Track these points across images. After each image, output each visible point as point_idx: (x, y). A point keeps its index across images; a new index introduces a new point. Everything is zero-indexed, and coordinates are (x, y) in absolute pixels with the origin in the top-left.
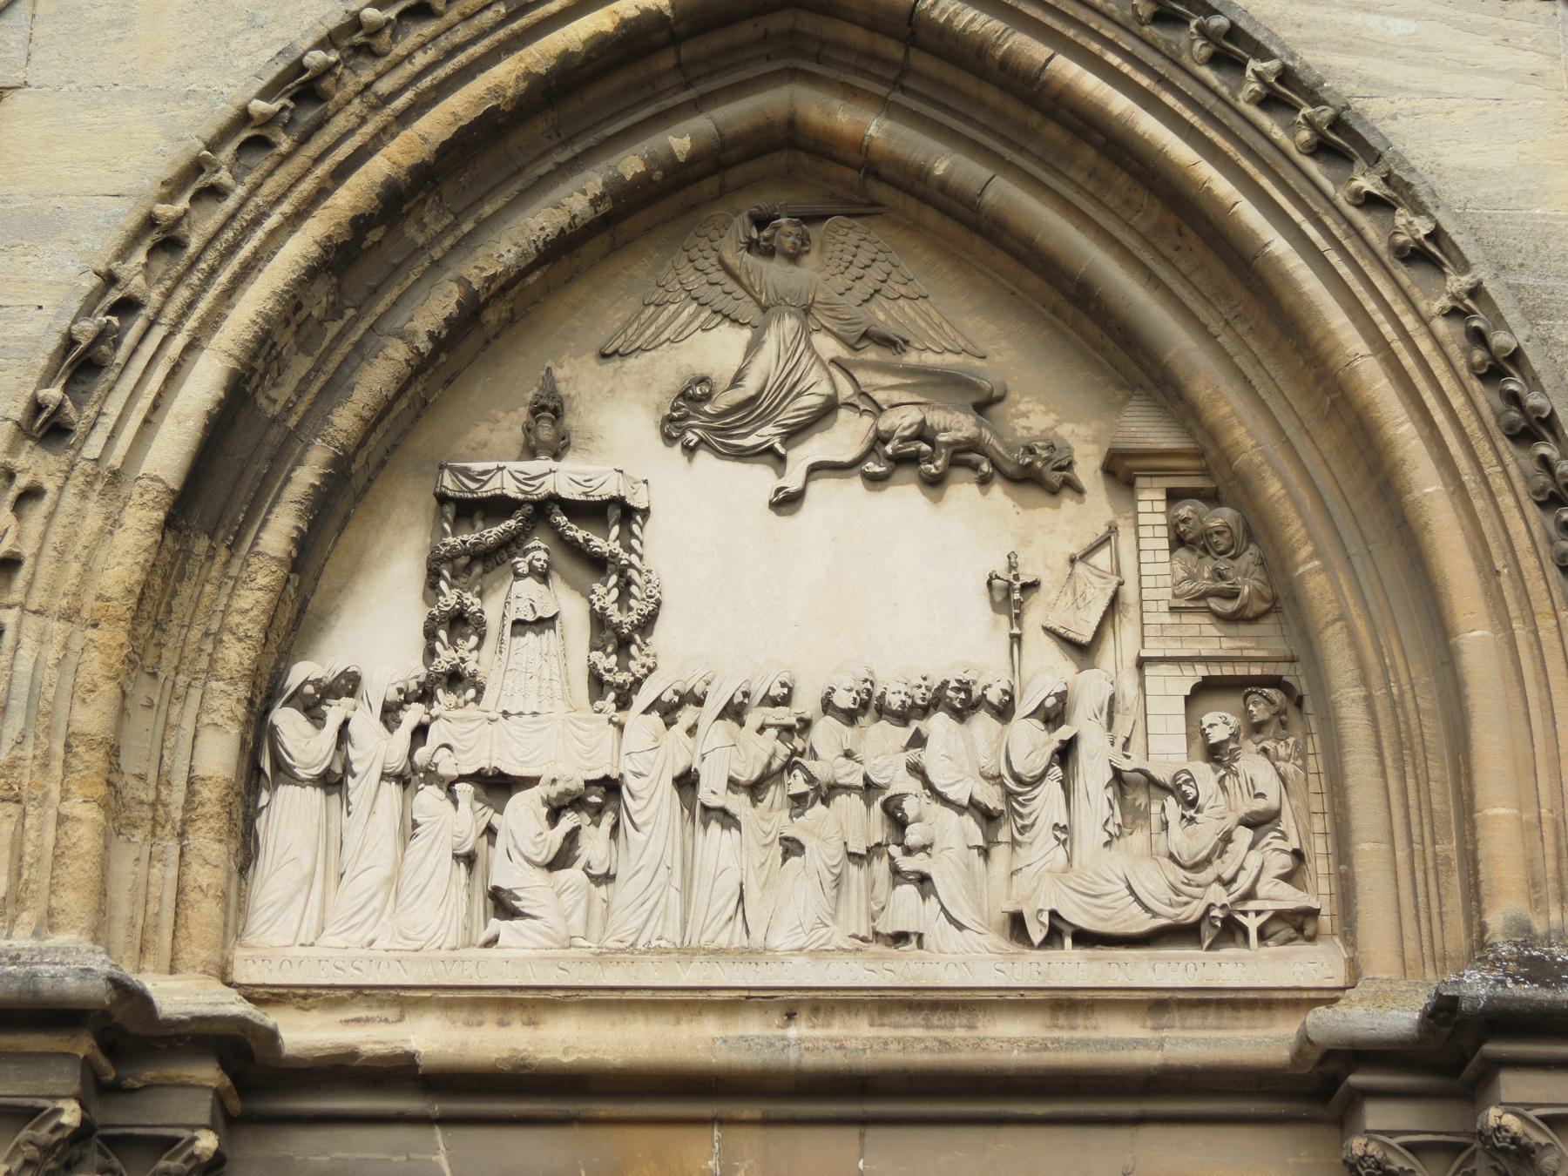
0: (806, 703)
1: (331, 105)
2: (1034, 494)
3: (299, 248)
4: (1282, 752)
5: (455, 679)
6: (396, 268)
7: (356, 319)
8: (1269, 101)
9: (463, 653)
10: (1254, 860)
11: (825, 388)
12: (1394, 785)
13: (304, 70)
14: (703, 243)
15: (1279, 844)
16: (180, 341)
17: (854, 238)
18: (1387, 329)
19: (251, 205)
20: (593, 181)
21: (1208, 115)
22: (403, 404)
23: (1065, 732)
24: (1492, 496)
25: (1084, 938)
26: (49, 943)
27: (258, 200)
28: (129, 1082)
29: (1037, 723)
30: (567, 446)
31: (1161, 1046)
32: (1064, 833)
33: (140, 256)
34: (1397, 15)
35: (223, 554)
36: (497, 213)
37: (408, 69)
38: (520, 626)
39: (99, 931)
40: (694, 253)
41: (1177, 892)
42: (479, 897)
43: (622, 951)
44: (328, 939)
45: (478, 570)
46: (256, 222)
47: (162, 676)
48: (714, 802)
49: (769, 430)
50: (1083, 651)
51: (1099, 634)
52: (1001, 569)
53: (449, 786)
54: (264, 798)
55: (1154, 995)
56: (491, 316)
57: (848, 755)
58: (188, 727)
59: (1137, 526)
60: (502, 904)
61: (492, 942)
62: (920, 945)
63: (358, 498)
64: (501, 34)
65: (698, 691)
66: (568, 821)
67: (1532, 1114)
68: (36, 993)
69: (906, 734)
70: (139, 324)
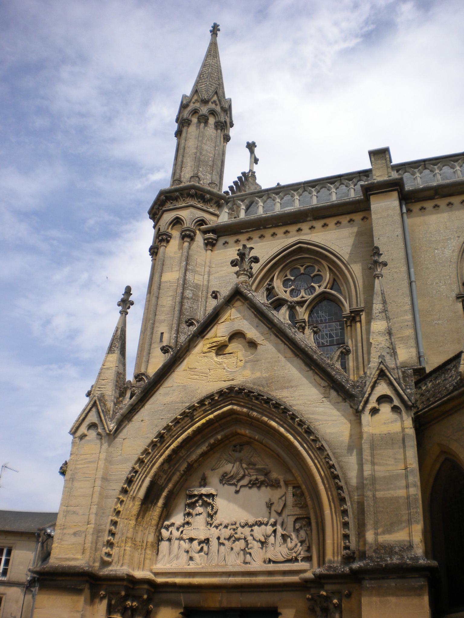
3: (161, 460)
5: (188, 523)
7: (173, 468)
11: (243, 473)
15: (305, 545)
16: (144, 476)
19: (154, 455)
20: (207, 444)
23: (275, 528)
25: (274, 562)
27: (155, 454)
38: (197, 515)
46: (155, 457)
53: (184, 540)
58: (147, 533)
64: (190, 424)
66: (202, 545)
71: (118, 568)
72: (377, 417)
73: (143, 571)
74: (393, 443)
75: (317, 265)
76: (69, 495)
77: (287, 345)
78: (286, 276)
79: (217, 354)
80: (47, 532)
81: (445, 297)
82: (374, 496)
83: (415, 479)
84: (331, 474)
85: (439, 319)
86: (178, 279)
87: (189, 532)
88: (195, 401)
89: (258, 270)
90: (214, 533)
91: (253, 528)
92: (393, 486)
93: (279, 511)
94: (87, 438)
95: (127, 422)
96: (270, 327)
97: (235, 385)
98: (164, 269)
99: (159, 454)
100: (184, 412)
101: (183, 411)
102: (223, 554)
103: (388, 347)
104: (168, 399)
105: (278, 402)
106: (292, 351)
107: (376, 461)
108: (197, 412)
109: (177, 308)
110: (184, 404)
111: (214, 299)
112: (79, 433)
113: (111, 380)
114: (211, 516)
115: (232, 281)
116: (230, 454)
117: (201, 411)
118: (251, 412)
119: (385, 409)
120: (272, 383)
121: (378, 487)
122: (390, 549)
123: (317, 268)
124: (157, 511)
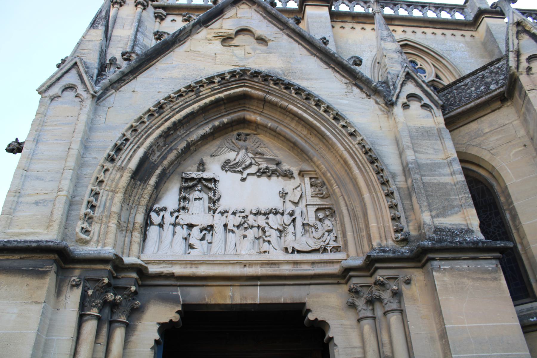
0: (247, 213)
2: (285, 178)
3: (158, 132)
5: (184, 208)
6: (175, 139)
7: (168, 147)
8: (325, 111)
9: (185, 204)
10: (329, 238)
11: (250, 161)
12: (353, 224)
13: (160, 103)
14: (229, 138)
15: (333, 235)
16: (136, 146)
19: (150, 125)
20: (210, 126)
21: (315, 114)
22: (176, 162)
23: (294, 217)
24: (368, 173)
25: (299, 252)
29: (288, 215)
30: (205, 170)
32: (295, 234)
33: (130, 132)
35: (142, 184)
36: (193, 130)
38: (196, 199)
39: (114, 247)
40: (227, 140)
42: (187, 246)
44: (159, 252)
46: (151, 128)
47: (130, 205)
48: (230, 229)
50: (296, 204)
52: (281, 190)
54: (148, 228)
55: (312, 261)
56: (192, 148)
57: (255, 221)
59: (305, 183)
60: (191, 247)
61: (189, 253)
62: (269, 253)
65: (228, 211)
66: (204, 232)
69: (265, 217)
70: (129, 143)
72: (409, 112)
77: (301, 45)
88: (203, 76)
90: (218, 221)
92: (437, 173)
94: (59, 99)
95: (114, 91)
106: (308, 50)
108: (204, 89)
114: (214, 201)
117: (208, 89)
118: (268, 96)
124: (149, 189)
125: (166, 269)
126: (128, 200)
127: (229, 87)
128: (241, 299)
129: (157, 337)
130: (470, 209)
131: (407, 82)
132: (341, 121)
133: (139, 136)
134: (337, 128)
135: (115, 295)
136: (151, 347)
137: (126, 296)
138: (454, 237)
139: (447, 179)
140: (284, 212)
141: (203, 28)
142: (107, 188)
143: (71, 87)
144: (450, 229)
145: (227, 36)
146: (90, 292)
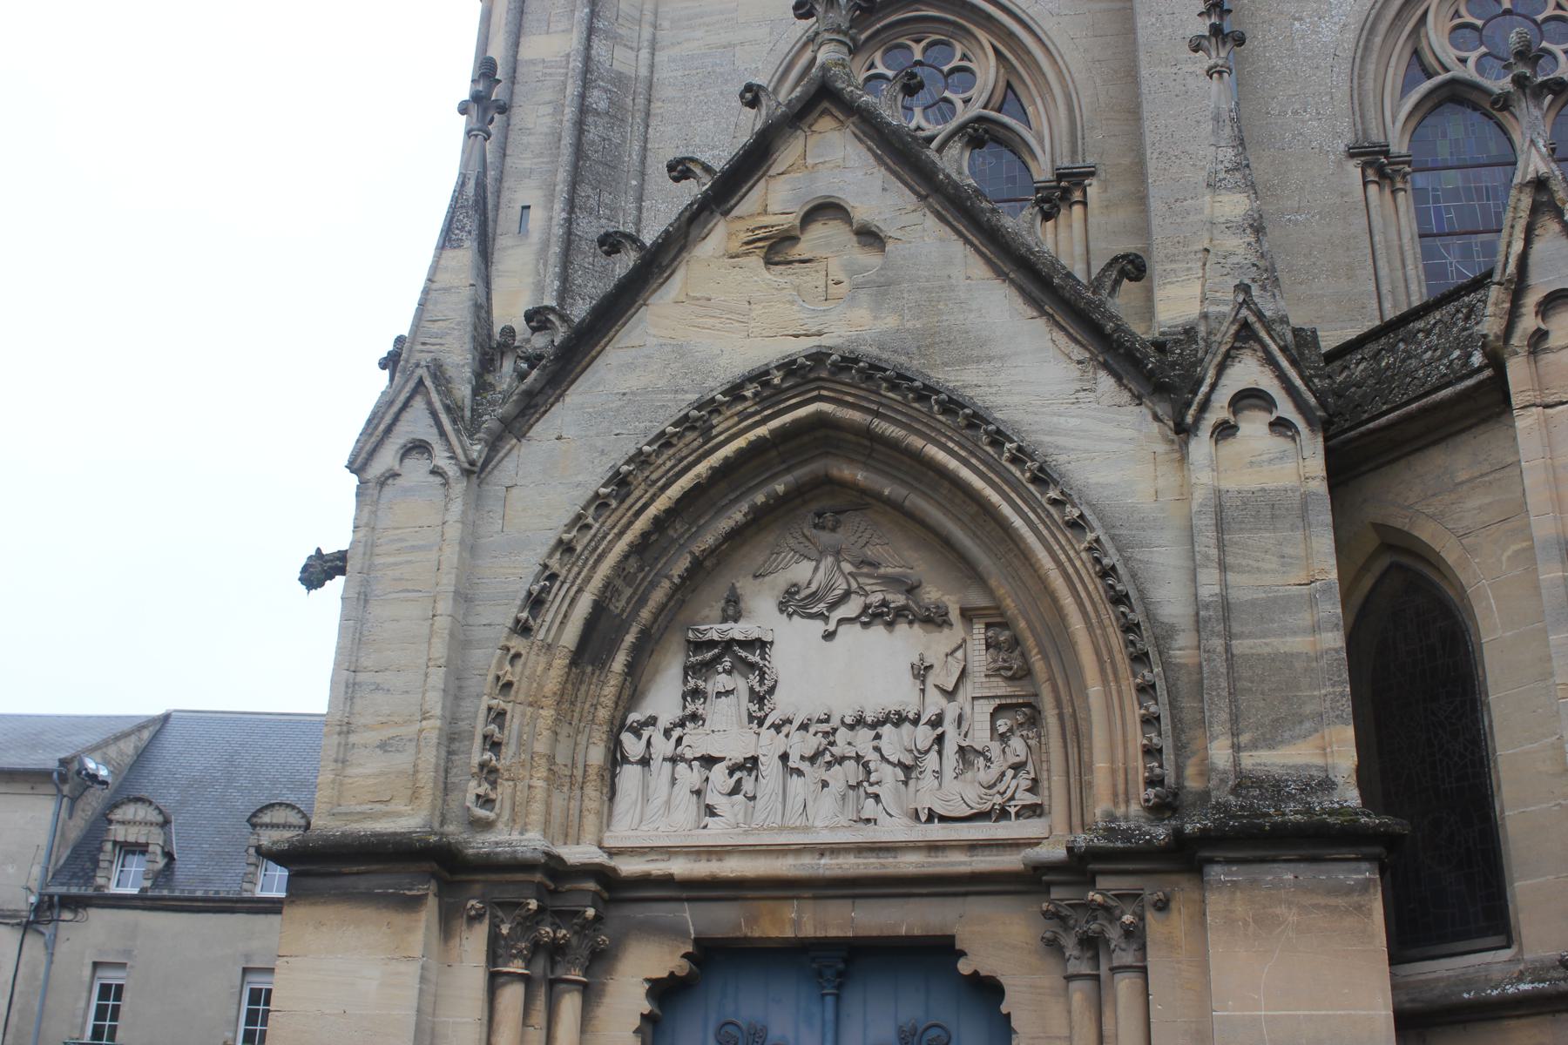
1: (632, 487)
2: (930, 627)
3: (621, 546)
4: (1030, 735)
5: (694, 717)
6: (665, 549)
7: (650, 571)
8: (1014, 460)
9: (697, 706)
10: (1014, 783)
11: (845, 586)
15: (1026, 776)
16: (575, 588)
17: (858, 519)
18: (1063, 557)
20: (745, 507)
23: (939, 731)
25: (943, 819)
26: (524, 837)
28: (560, 889)
29: (928, 727)
30: (740, 616)
31: (970, 865)
32: (938, 774)
33: (558, 555)
34: (1073, 417)
35: (597, 672)
36: (706, 522)
37: (663, 469)
38: (719, 694)
39: (545, 833)
40: (792, 531)
41: (981, 799)
42: (703, 808)
43: (757, 829)
45: (704, 671)
46: (604, 537)
48: (794, 766)
49: (822, 605)
50: (950, 695)
51: (956, 686)
53: (689, 762)
56: (708, 563)
57: (849, 744)
58: (584, 743)
60: (711, 811)
62: (875, 824)
63: (657, 642)
64: (701, 451)
66: (737, 775)
67: (1109, 893)
68: (516, 858)
69: (873, 733)
70: (558, 584)
71: (515, 836)
72: (1230, 447)
73: (565, 844)
74: (1273, 517)
75: (960, 42)
76: (360, 640)
78: (872, 66)
79: (769, 262)
80: (86, 769)
81: (1317, 150)
82: (1228, 649)
83: (1332, 609)
84: (1106, 592)
85: (1298, 211)
86: (568, 55)
87: (698, 741)
88: (714, 385)
89: (794, 46)
90: (768, 745)
91: (880, 730)
93: (950, 688)
94: (399, 481)
95: (514, 441)
96: (924, 193)
97: (831, 349)
98: (526, 25)
99: (616, 531)
100: (686, 416)
101: (682, 413)
102: (800, 800)
103: (1254, 265)
104: (633, 382)
105: (955, 397)
106: (988, 261)
107: (1230, 560)
108: (720, 418)
109: (567, 140)
110: (680, 397)
111: (748, 109)
112: (377, 468)
113: (458, 324)
114: (758, 698)
115: (722, 70)
116: (805, 536)
117: (732, 416)
118: (876, 421)
119: (1254, 426)
120: (932, 345)
121: (1236, 628)
122: (1273, 786)
123: (959, 49)
124: (612, 683)
125: (657, 867)
126: (570, 714)
127: (782, 406)
128: (815, 927)
129: (646, 1007)
130: (1340, 727)
131: (1242, 351)
132: (1052, 486)
133: (580, 563)
134: (1041, 505)
135: (556, 928)
136: (634, 1029)
137: (577, 928)
138: (1282, 801)
139: (1299, 644)
140: (919, 716)
141: (718, 216)
142: (521, 697)
143: (419, 447)
144: (1277, 781)
145: (780, 236)
146: (505, 930)
